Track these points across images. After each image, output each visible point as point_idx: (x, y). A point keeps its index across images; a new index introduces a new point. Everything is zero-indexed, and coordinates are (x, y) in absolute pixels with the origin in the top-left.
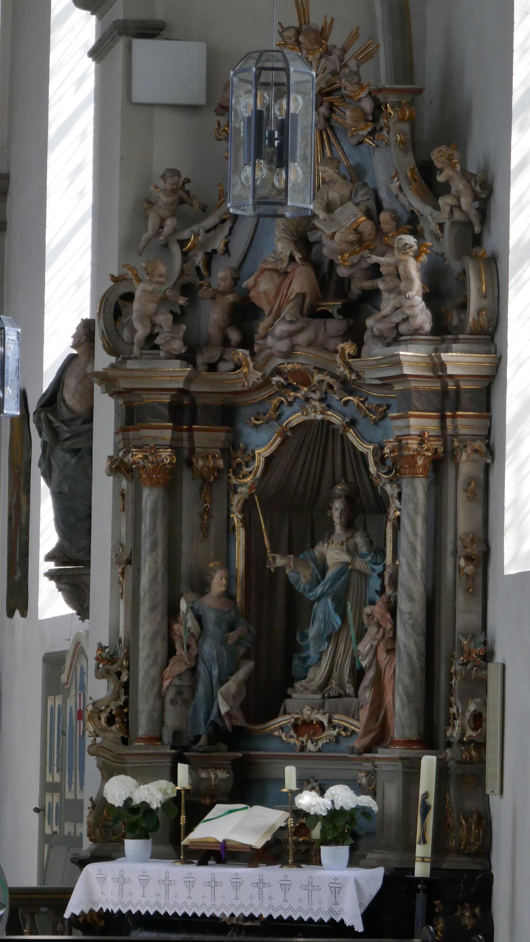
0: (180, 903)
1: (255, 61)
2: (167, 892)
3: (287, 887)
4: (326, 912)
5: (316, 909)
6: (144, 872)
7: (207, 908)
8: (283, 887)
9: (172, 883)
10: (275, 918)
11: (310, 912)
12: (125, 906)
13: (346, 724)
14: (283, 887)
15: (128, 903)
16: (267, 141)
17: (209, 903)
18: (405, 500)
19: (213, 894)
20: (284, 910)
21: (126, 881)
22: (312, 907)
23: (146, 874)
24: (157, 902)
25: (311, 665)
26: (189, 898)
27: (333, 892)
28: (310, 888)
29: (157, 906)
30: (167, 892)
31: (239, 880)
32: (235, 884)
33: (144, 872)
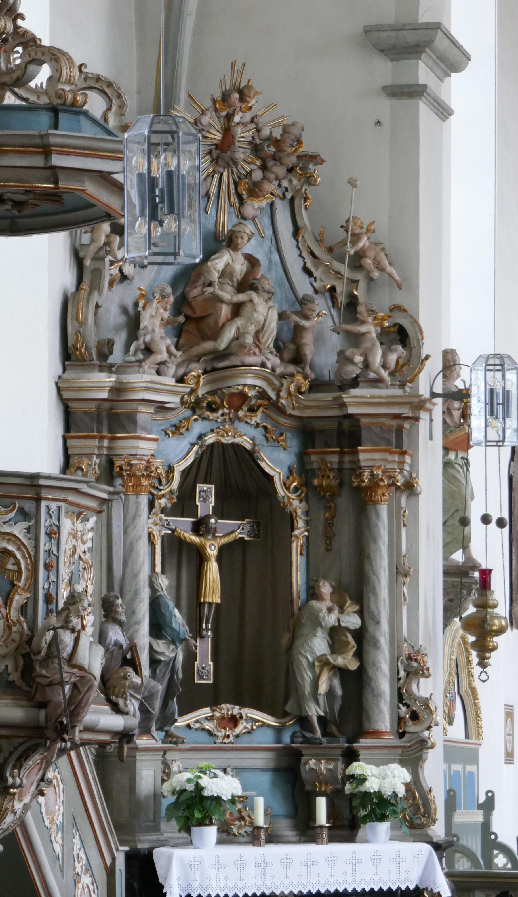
0: (278, 883)
1: (148, 125)
2: (399, 868)
3: (334, 862)
4: (323, 883)
5: (403, 879)
6: (240, 856)
7: (239, 889)
8: (238, 866)
9: (269, 865)
10: (376, 890)
11: (236, 889)
12: (258, 889)
13: (203, 716)
14: (330, 863)
15: (353, 882)
16: (157, 193)
17: (350, 879)
18: (154, 514)
19: (354, 870)
20: (339, 884)
21: (222, 866)
22: (400, 877)
23: (242, 859)
24: (345, 880)
25: (448, 628)
26: (376, 874)
27: (239, 869)
28: (354, 861)
29: (226, 889)
30: (399, 868)
31: (243, 862)
32: (284, 864)
33: (240, 856)
